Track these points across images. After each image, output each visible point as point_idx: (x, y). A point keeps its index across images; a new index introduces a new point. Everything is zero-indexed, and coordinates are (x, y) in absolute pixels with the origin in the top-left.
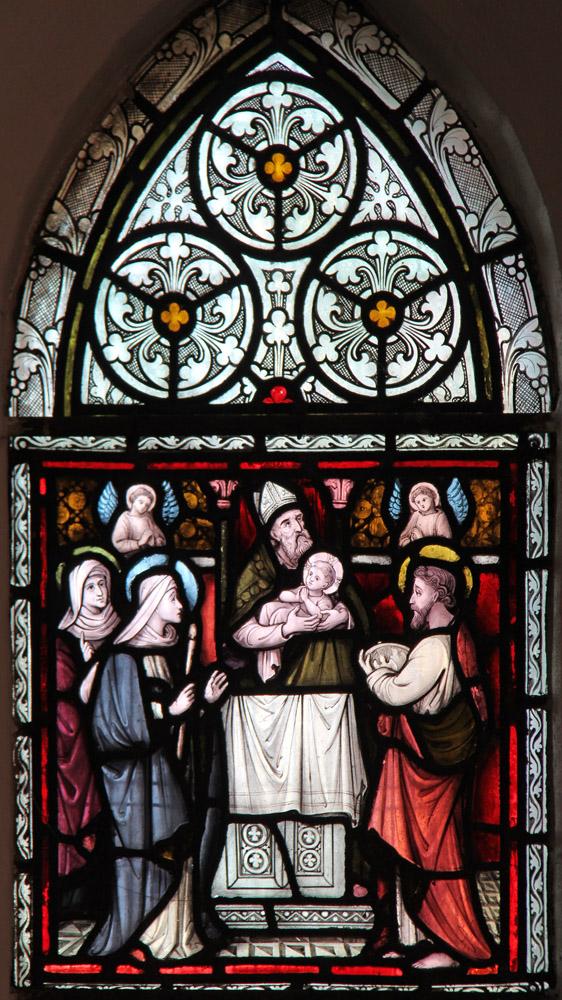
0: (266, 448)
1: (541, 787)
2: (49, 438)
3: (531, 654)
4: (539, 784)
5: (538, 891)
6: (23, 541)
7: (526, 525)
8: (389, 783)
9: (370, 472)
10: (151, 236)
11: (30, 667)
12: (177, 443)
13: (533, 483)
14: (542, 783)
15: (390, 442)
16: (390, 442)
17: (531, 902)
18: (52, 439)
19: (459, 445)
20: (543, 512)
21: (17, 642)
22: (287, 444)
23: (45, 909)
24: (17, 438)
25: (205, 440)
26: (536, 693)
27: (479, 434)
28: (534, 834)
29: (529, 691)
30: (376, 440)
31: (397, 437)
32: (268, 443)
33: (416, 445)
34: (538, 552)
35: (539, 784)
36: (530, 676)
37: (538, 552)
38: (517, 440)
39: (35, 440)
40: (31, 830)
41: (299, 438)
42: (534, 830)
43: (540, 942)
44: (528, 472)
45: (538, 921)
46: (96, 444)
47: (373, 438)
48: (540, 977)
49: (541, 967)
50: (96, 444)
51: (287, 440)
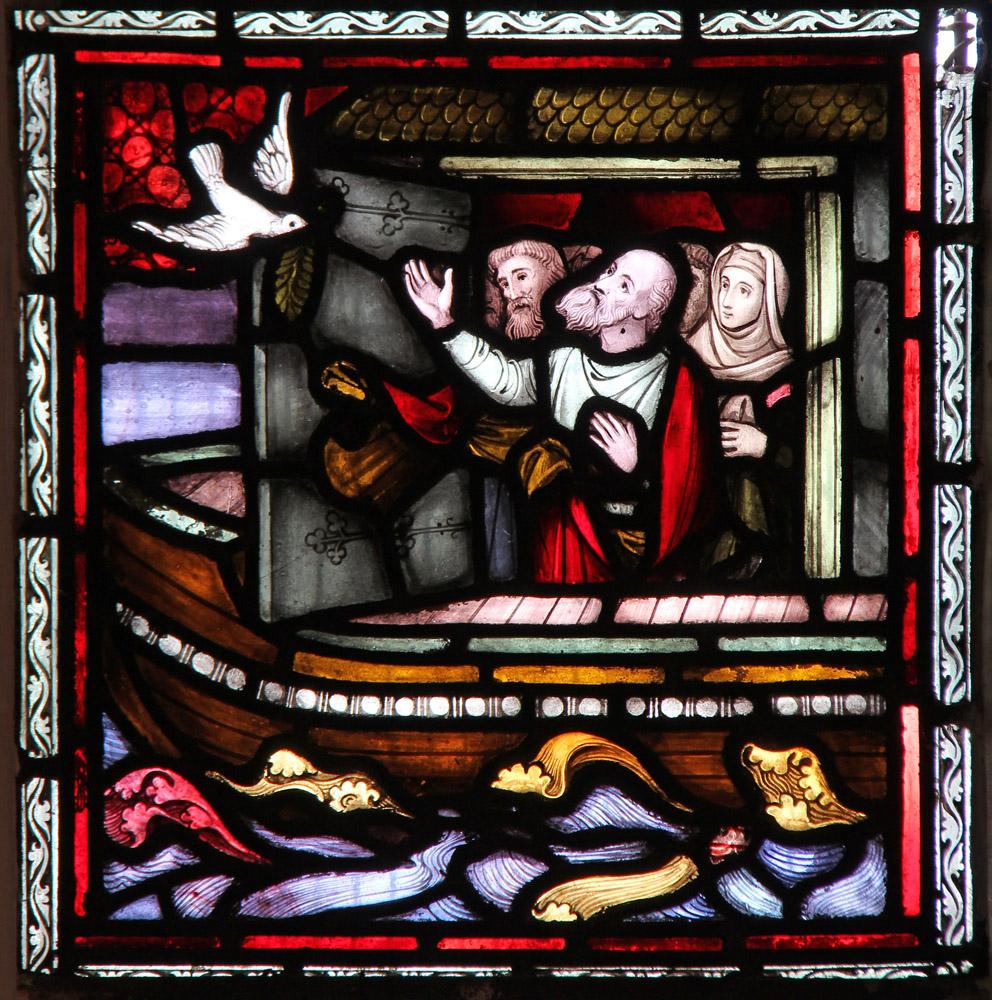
0: (466, 32)
1: (963, 382)
5: (954, 400)
7: (935, 386)
8: (601, 884)
12: (618, 23)
13: (944, 510)
15: (457, 26)
16: (690, 26)
17: (943, 266)
20: (963, 144)
22: (273, 26)
25: (593, 20)
30: (430, 20)
31: (469, 15)
32: (470, 26)
33: (271, 31)
34: (958, 215)
36: (946, 912)
37: (958, 215)
38: (407, 266)
39: (136, 18)
41: (521, 15)
44: (938, 331)
46: (164, 21)
49: (959, 454)
50: (164, 21)
51: (273, 20)
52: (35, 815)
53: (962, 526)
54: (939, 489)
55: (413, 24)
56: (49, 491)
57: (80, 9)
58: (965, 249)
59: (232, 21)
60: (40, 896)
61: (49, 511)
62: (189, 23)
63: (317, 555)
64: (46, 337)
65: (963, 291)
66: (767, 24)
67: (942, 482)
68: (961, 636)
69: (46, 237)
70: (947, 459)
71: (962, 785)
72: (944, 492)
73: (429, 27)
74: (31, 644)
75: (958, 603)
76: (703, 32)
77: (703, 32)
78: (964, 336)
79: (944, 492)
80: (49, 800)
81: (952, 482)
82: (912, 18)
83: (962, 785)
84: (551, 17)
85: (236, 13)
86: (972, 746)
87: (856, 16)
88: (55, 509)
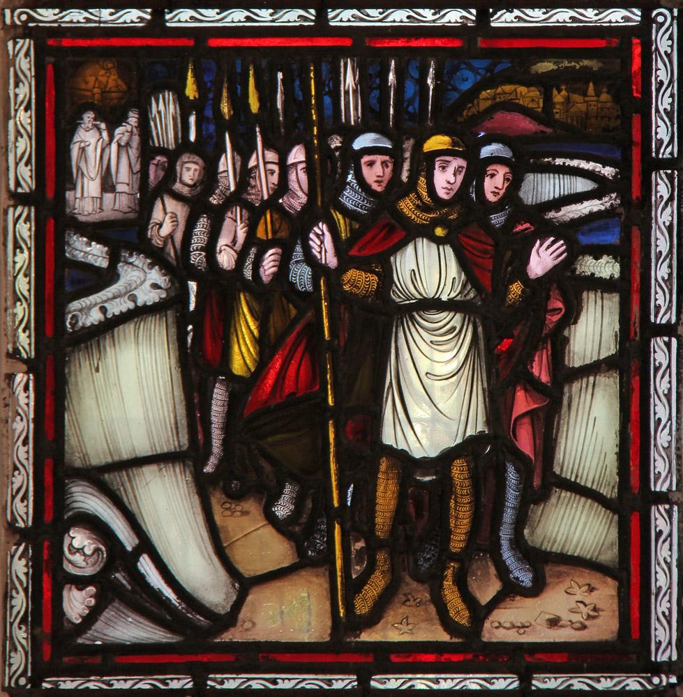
2: (57, 11)
3: (660, 611)
4: (667, 598)
6: (25, 136)
9: (453, 53)
10: (121, 689)
11: (32, 404)
14: (670, 597)
18: (61, 12)
19: (568, 20)
20: (672, 46)
21: (17, 259)
23: (97, 25)
24: (19, 11)
26: (667, 156)
27: (594, 7)
28: (660, 324)
29: (657, 152)
32: (331, 15)
35: (667, 598)
38: (639, 13)
40: (30, 610)
42: (662, 319)
43: (668, 124)
45: (664, 541)
47: (623, 12)
48: (667, 668)
52: (19, 455)
53: (671, 82)
54: (656, 174)
55: (291, 17)
56: (29, 174)
57: (53, 7)
58: (670, 340)
59: (163, 14)
60: (22, 450)
61: (30, 189)
62: (132, 16)
63: (221, 518)
64: (27, 341)
65: (669, 539)
66: (536, 16)
67: (657, 169)
68: (669, 276)
69: (28, 278)
70: (658, 322)
71: (670, 382)
72: (658, 343)
73: (626, 19)
74: (14, 504)
75: (667, 587)
76: (167, 21)
77: (167, 21)
78: (671, 121)
79: (658, 343)
80: (28, 444)
81: (661, 335)
82: (636, 15)
83: (670, 382)
84: (547, 12)
85: (166, 10)
86: (679, 571)
87: (597, 12)
88: (34, 187)
